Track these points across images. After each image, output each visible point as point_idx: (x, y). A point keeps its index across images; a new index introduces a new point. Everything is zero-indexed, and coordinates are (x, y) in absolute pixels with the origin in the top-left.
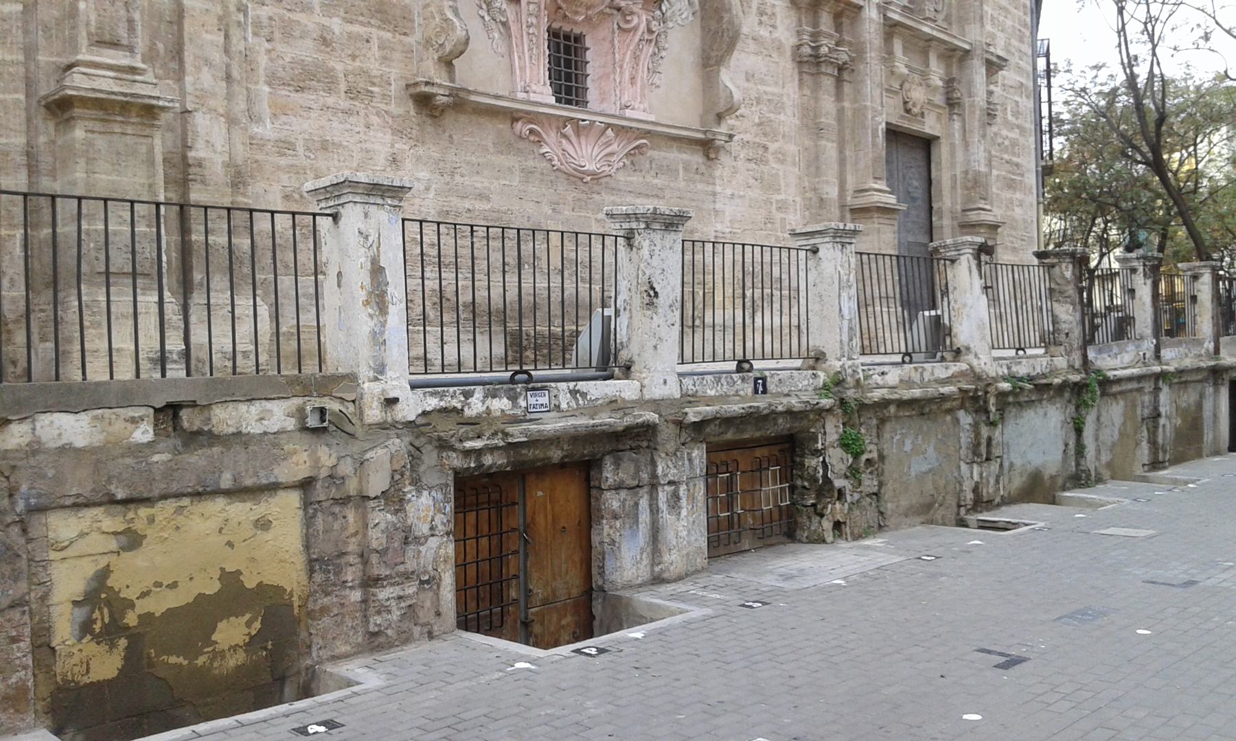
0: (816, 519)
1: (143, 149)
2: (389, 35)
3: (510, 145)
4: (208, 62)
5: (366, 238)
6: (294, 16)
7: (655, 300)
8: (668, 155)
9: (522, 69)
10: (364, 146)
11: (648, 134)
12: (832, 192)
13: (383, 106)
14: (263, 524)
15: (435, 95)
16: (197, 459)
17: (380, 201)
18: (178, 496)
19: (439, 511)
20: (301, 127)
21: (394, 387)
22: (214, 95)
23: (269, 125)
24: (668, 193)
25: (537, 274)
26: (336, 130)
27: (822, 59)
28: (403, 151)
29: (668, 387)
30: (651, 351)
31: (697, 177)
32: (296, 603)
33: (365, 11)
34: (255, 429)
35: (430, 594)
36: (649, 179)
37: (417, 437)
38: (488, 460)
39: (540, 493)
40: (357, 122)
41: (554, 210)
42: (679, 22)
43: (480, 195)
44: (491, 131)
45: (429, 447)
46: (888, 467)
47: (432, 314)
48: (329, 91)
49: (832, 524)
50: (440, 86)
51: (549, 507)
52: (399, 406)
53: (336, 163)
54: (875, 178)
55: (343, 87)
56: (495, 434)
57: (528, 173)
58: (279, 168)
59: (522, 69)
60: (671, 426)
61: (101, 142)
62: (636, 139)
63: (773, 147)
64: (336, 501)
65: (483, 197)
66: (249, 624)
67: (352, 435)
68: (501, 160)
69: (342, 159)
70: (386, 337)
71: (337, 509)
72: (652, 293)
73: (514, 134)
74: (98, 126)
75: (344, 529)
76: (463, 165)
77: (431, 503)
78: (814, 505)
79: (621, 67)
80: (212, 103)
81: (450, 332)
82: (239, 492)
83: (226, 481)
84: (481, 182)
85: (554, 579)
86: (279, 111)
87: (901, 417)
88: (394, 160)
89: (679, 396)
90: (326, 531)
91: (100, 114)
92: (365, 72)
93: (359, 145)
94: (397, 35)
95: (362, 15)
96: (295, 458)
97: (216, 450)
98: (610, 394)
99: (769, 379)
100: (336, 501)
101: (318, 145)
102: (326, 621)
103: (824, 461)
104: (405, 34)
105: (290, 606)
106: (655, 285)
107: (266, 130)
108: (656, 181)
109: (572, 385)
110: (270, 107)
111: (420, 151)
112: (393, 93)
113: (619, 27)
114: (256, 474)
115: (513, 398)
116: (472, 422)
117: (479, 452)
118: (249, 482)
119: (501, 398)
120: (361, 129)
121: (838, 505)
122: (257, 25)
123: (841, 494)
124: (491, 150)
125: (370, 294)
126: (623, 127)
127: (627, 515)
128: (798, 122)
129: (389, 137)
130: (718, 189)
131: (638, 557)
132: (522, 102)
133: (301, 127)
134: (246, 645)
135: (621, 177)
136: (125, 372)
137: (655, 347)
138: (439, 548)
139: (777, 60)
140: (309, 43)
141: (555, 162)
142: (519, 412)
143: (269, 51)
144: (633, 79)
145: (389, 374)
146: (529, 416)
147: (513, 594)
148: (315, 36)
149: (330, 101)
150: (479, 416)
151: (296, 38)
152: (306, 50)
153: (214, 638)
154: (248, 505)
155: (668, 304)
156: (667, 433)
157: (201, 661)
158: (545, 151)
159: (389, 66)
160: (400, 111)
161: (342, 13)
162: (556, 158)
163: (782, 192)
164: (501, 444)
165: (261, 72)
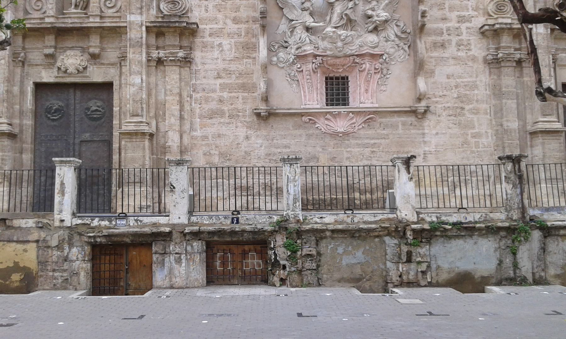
0: (272, 276)
1: (142, 145)
2: (246, 94)
3: (301, 126)
4: (173, 115)
5: (60, 175)
6: (209, 95)
7: (173, 190)
8: (391, 120)
9: (305, 96)
10: (235, 134)
11: (375, 113)
12: (514, 125)
13: (243, 119)
14: (25, 251)
15: (260, 113)
16: (8, 233)
17: (65, 165)
18: (4, 241)
19: (80, 253)
20: (210, 131)
21: (64, 217)
22: (175, 125)
23: (199, 131)
24: (391, 137)
25: (313, 175)
26: (224, 130)
27: (500, 60)
28: (251, 134)
29: (181, 219)
30: (173, 207)
31: (411, 127)
32: (34, 273)
33: (237, 88)
34: (24, 226)
35: (77, 277)
36: (379, 131)
37: (71, 231)
38: (98, 240)
39: (134, 253)
40: (232, 127)
41: (323, 149)
42: (399, 60)
43: (286, 146)
44: (290, 123)
45: (76, 234)
46: (323, 259)
47: (262, 192)
48: (222, 117)
49: (279, 279)
50: (261, 109)
51: (138, 258)
52: (65, 222)
53: (224, 141)
54: (544, 115)
55: (227, 115)
56: (99, 232)
57: (309, 136)
58: (202, 145)
59: (305, 96)
60: (179, 234)
61: (129, 145)
62: (369, 115)
63: (467, 107)
64: (45, 247)
65: (286, 147)
66: (20, 276)
67: (50, 229)
68: (298, 132)
69: (226, 139)
70: (63, 202)
71: (46, 249)
72: (172, 187)
73: (303, 121)
74: (128, 140)
75: (48, 255)
76: (278, 136)
77: (77, 250)
78: (271, 270)
79: (360, 86)
80: (174, 128)
81: (268, 198)
82: (18, 242)
83: (15, 238)
84: (285, 142)
85: (140, 281)
86: (203, 126)
87: (334, 237)
88: (247, 138)
89: (187, 223)
90: (42, 255)
91: (129, 136)
92: (237, 109)
93: (233, 134)
94: (250, 94)
95: (236, 89)
96: (34, 234)
97: (13, 231)
98: (153, 221)
99: (240, 218)
100: (45, 247)
101: (217, 136)
102: (42, 279)
103: (275, 253)
104: (253, 93)
105: (33, 273)
106: (173, 184)
107: (198, 133)
108: (384, 132)
109: (136, 218)
110: (200, 125)
111: (259, 133)
112: (247, 114)
113: (359, 71)
114: (23, 237)
115: (110, 221)
116: (93, 228)
117: (94, 237)
118: (21, 239)
119: (105, 221)
120: (234, 128)
121: (282, 272)
122: (196, 100)
123: (284, 267)
124: (291, 129)
125: (59, 191)
126: (360, 111)
127: (159, 263)
128: (489, 93)
129: (245, 130)
130: (426, 131)
131: (164, 278)
132: (304, 109)
133: (210, 131)
134: (20, 281)
135: (362, 132)
136: (131, 210)
137: (175, 206)
138: (80, 264)
139: (472, 65)
140: (215, 102)
141: (323, 130)
142: (112, 226)
143: (200, 108)
144: (367, 91)
145: (64, 213)
146: (116, 227)
147: (122, 284)
148: (217, 100)
149: (222, 120)
150: (96, 226)
151: (209, 102)
152: (213, 105)
153: (11, 277)
154: (22, 245)
155: (180, 190)
156: (175, 235)
157: (7, 283)
158: (317, 126)
159: (246, 105)
160: (250, 120)
161: (228, 90)
162: (323, 128)
163: (476, 128)
164: (101, 235)
165: (197, 115)
